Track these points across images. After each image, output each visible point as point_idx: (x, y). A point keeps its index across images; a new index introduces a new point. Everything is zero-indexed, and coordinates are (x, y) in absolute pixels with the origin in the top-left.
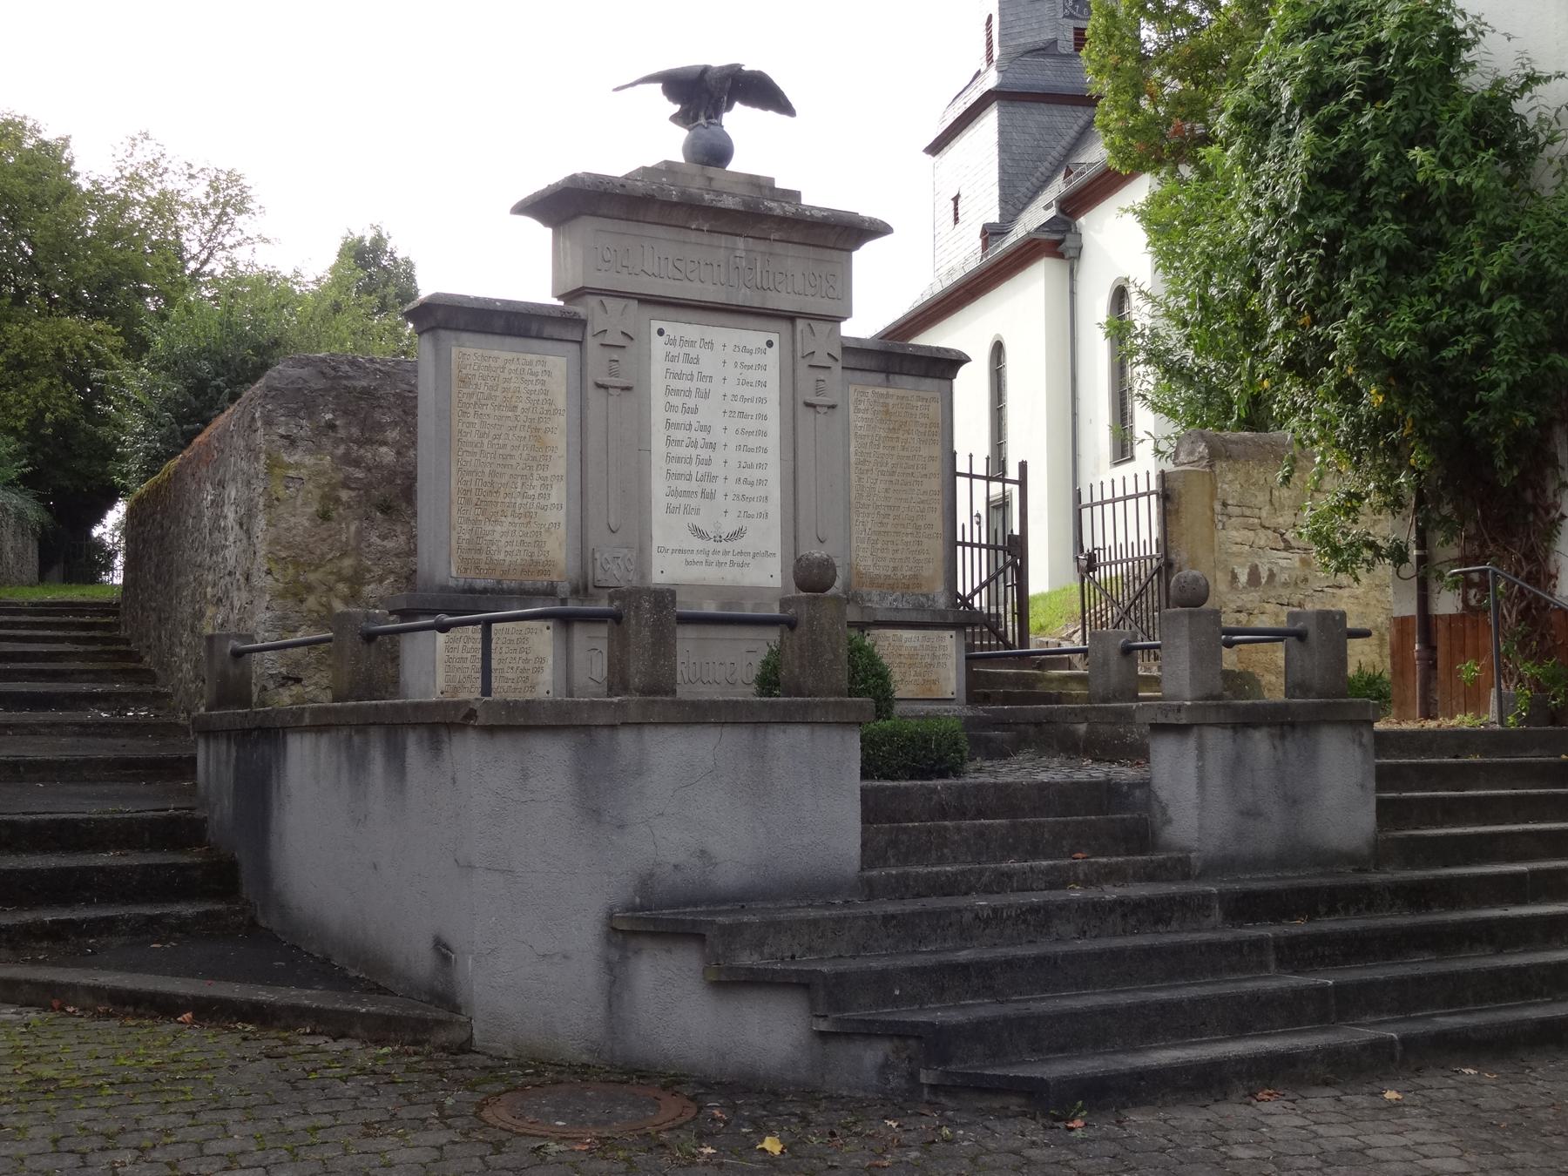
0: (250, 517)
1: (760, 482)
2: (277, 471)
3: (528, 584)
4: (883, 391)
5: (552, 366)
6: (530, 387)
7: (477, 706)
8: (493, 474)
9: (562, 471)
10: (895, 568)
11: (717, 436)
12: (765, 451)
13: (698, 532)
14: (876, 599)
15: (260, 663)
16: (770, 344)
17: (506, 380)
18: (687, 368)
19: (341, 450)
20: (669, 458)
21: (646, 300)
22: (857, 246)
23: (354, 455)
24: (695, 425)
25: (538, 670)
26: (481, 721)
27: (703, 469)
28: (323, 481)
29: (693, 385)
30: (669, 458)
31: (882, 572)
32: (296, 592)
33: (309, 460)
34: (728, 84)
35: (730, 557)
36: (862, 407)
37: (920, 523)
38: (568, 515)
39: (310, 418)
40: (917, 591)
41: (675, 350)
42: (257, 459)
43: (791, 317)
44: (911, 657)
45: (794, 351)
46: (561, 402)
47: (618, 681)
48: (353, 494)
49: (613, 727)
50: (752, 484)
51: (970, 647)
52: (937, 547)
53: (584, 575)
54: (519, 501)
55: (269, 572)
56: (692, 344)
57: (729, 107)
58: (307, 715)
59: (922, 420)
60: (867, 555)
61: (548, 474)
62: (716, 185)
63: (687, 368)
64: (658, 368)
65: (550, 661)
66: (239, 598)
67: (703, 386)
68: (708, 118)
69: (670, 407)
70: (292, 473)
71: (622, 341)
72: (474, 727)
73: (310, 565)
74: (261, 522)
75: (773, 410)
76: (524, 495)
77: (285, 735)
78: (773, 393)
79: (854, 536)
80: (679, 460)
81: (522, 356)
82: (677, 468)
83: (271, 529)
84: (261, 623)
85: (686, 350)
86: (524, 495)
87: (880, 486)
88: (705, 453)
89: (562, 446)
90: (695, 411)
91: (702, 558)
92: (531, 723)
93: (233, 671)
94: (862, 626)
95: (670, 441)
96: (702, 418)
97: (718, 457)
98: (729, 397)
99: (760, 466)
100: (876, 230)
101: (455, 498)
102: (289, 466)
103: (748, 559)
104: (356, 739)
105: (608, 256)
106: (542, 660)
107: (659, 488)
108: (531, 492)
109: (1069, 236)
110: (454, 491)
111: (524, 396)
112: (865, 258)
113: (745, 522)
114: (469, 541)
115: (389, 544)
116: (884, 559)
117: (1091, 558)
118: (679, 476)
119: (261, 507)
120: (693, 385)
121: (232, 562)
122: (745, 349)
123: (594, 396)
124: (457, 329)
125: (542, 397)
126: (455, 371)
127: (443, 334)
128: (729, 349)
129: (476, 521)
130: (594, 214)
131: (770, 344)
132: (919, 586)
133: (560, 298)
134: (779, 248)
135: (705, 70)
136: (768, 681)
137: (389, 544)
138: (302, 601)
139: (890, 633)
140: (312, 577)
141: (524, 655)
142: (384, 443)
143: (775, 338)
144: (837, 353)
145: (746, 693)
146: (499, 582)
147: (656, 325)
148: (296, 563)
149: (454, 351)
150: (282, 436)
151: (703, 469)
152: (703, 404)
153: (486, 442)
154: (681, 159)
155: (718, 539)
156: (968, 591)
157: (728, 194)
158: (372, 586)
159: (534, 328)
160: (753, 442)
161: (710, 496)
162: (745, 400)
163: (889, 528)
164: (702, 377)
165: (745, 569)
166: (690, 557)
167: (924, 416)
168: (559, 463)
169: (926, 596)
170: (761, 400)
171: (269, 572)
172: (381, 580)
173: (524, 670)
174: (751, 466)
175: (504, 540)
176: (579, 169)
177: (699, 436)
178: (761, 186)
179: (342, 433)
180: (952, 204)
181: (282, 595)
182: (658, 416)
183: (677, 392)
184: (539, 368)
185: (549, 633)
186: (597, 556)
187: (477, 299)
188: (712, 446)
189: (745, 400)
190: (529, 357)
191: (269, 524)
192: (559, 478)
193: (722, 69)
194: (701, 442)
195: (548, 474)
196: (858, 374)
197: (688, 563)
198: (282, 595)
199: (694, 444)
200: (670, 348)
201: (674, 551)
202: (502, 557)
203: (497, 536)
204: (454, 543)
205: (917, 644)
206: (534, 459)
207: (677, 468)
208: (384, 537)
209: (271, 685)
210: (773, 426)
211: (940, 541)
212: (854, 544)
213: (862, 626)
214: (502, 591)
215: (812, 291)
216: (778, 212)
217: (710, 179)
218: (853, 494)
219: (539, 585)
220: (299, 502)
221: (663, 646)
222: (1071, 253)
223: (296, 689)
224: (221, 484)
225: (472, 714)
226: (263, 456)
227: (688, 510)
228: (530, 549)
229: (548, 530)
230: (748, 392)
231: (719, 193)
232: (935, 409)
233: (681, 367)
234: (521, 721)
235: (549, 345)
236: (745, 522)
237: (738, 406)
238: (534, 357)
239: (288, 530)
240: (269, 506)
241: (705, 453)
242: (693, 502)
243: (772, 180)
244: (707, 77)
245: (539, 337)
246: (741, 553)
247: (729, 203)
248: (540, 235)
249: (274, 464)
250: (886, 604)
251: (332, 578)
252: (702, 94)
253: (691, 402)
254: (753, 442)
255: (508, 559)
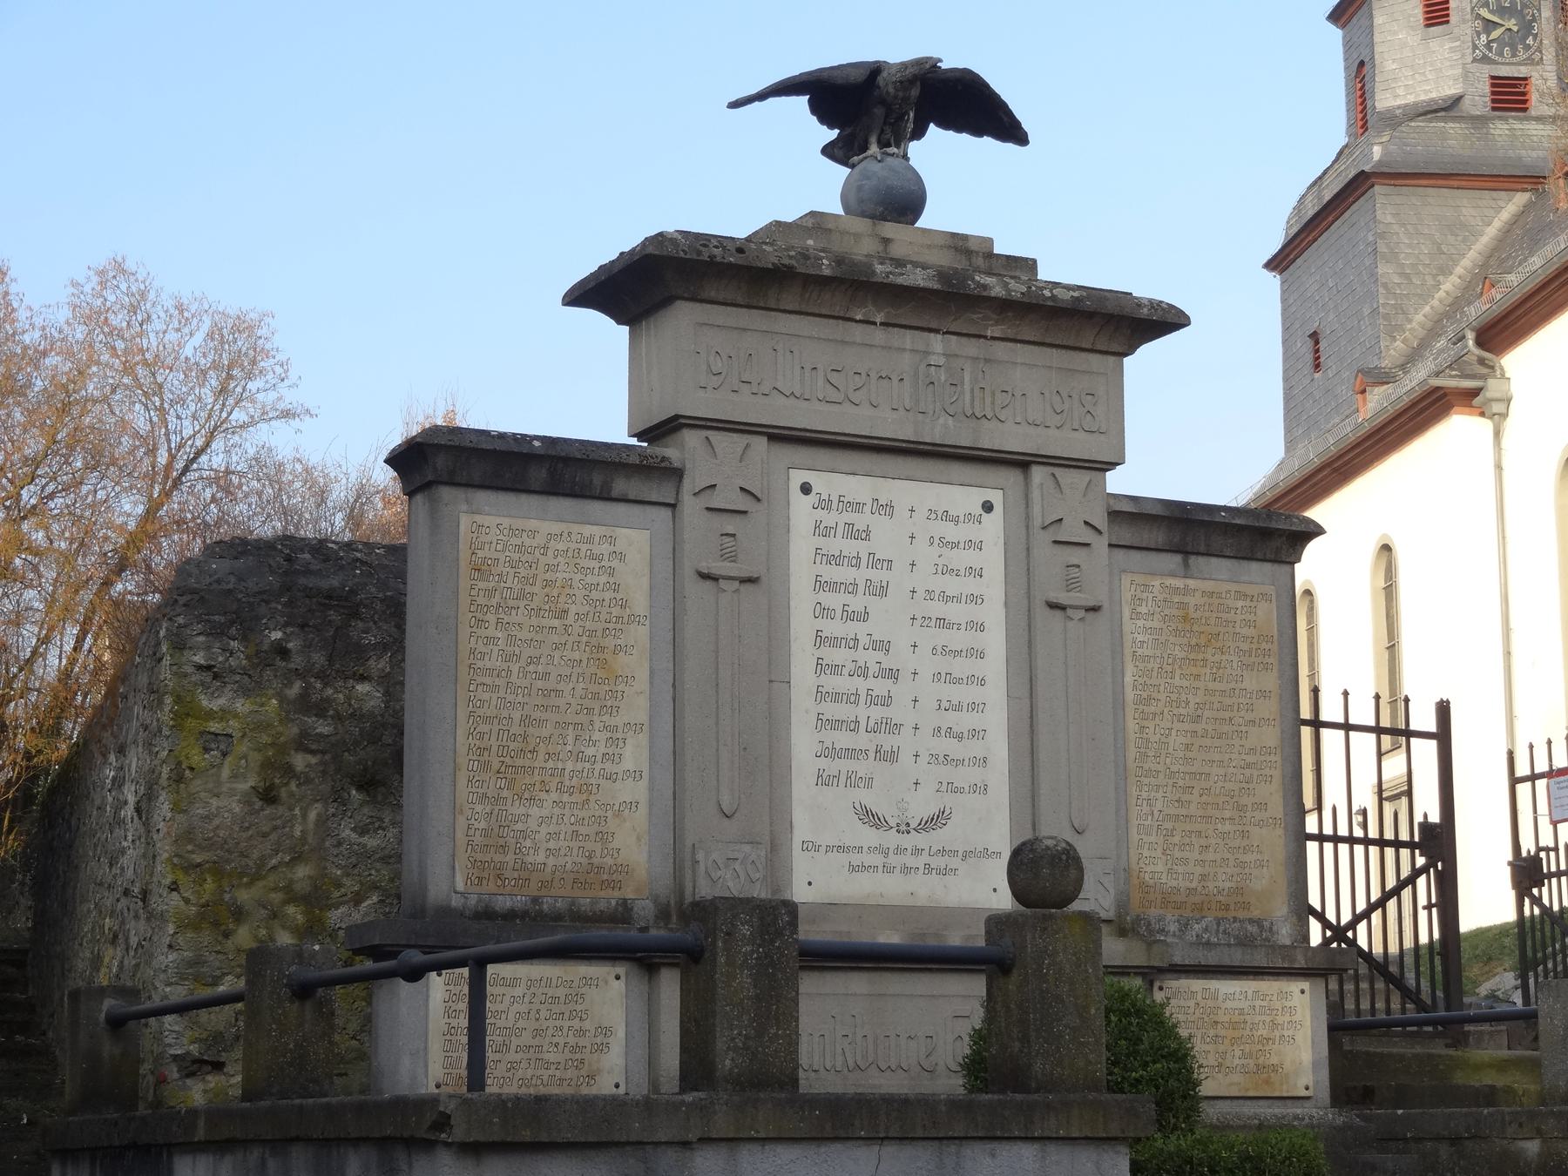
0: (150, 799)
1: (974, 733)
2: (191, 723)
3: (585, 904)
4: (1178, 583)
5: (621, 548)
6: (589, 579)
7: (450, 1107)
8: (526, 720)
9: (642, 716)
10: (1204, 877)
11: (900, 658)
12: (982, 682)
13: (870, 817)
14: (1173, 928)
15: (158, 1037)
16: (988, 507)
17: (549, 568)
18: (851, 547)
19: (295, 690)
20: (821, 695)
21: (781, 437)
22: (1130, 350)
23: (315, 698)
24: (864, 640)
25: (602, 1048)
26: (459, 1133)
27: (877, 713)
28: (265, 739)
29: (861, 575)
30: (821, 695)
31: (1183, 884)
32: (217, 918)
33: (242, 706)
34: (915, 92)
35: (924, 858)
36: (1143, 610)
37: (1245, 800)
38: (651, 789)
39: (244, 639)
40: (1241, 915)
41: (829, 519)
42: (161, 702)
43: (1022, 463)
44: (1234, 1025)
45: (1028, 517)
46: (640, 604)
47: (697, 1066)
48: (313, 760)
49: (685, 1145)
50: (960, 737)
51: (1335, 1008)
52: (1274, 840)
53: (680, 891)
54: (569, 766)
55: (174, 887)
56: (858, 507)
57: (919, 133)
58: (201, 1123)
59: (1245, 631)
60: (1145, 854)
61: (618, 720)
62: (897, 251)
63: (851, 547)
64: (801, 547)
65: (621, 1033)
66: (136, 930)
67: (877, 575)
68: (883, 144)
69: (823, 612)
70: (214, 727)
71: (741, 503)
72: (447, 1145)
73: (241, 875)
74: (163, 806)
75: (994, 614)
76: (578, 756)
77: (170, 1156)
78: (993, 587)
79: (1134, 822)
80: (837, 697)
81: (575, 528)
82: (832, 710)
83: (180, 818)
84: (164, 973)
85: (849, 517)
86: (578, 756)
87: (1176, 741)
88: (881, 687)
89: (643, 675)
90: (864, 616)
91: (877, 860)
92: (544, 1138)
93: (109, 1049)
94: (1152, 974)
95: (821, 666)
96: (877, 627)
97: (902, 691)
98: (921, 593)
99: (973, 707)
100: (1160, 321)
101: (462, 760)
102: (210, 715)
103: (954, 862)
104: (272, 1164)
105: (718, 365)
106: (607, 1031)
107: (803, 743)
108: (590, 751)
109: (1491, 382)
110: (462, 749)
111: (580, 594)
112: (1145, 365)
113: (949, 800)
114: (486, 833)
115: (371, 842)
116: (1185, 861)
117: (1535, 861)
118: (836, 724)
119: (164, 781)
120: (861, 575)
121: (130, 873)
122: (946, 516)
123: (696, 591)
124: (469, 485)
125: (608, 595)
126: (464, 554)
127: (446, 493)
128: (921, 513)
129: (498, 799)
130: (694, 299)
131: (988, 507)
132: (1246, 906)
133: (640, 436)
134: (1001, 350)
135: (875, 70)
136: (978, 1068)
137: (371, 842)
138: (227, 935)
139: (1197, 985)
140: (244, 896)
141: (576, 1023)
142: (363, 678)
143: (996, 497)
144: (1100, 521)
145: (952, 1084)
146: (535, 900)
147: (798, 477)
148: (218, 871)
149: (465, 521)
150: (200, 667)
151: (877, 713)
152: (875, 604)
153: (515, 668)
154: (841, 212)
155: (905, 828)
156: (1346, 917)
157: (916, 264)
158: (342, 909)
159: (597, 479)
160: (961, 667)
161: (891, 757)
162: (946, 598)
163: (1193, 810)
164: (875, 562)
165: (950, 878)
166: (856, 859)
167: (1248, 624)
168: (636, 706)
169: (1258, 922)
170: (975, 599)
171: (174, 887)
172: (357, 900)
173: (576, 1048)
174: (958, 708)
175: (544, 830)
176: (671, 223)
177: (871, 658)
178: (969, 251)
179: (297, 661)
180: (1310, 343)
181: (193, 925)
182: (802, 625)
183: (834, 586)
184: (605, 548)
185: (618, 987)
186: (700, 856)
187: (502, 436)
188: (893, 674)
189: (946, 598)
190: (588, 530)
191: (176, 808)
192: (637, 728)
193: (904, 65)
194: (874, 668)
195: (618, 720)
196: (1136, 556)
197: (853, 868)
198: (193, 925)
199: (863, 672)
200: (820, 514)
201: (829, 849)
202: (541, 858)
203: (533, 824)
204: (460, 835)
205: (1244, 1005)
206: (596, 696)
207: (832, 710)
208: (363, 831)
209: (173, 1072)
210: (995, 641)
211: (1280, 831)
212: (1134, 835)
213: (1152, 974)
214: (541, 916)
215: (1057, 420)
216: (997, 291)
217: (886, 241)
218: (1132, 753)
219: (602, 906)
220: (226, 773)
221: (775, 1009)
222: (1497, 407)
223: (213, 1080)
224: (121, 751)
225: (443, 1122)
226: (168, 700)
227: (852, 781)
228: (589, 846)
229: (618, 814)
230: (953, 585)
231: (900, 263)
232: (1267, 613)
233: (836, 545)
234: (527, 1135)
235: (621, 509)
236: (949, 800)
237: (937, 609)
238: (596, 531)
239: (207, 818)
240: (178, 778)
241: (881, 687)
242: (862, 767)
243: (990, 241)
244: (880, 80)
245: (606, 497)
246: (942, 852)
247: (918, 278)
248: (606, 336)
249: (186, 711)
250: (1191, 936)
251: (277, 897)
252: (868, 108)
253: (857, 603)
254: (961, 667)
255: (551, 861)
